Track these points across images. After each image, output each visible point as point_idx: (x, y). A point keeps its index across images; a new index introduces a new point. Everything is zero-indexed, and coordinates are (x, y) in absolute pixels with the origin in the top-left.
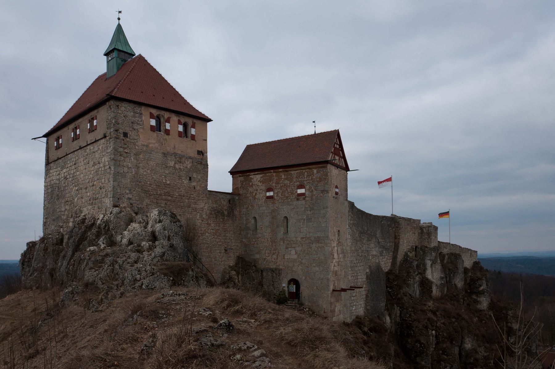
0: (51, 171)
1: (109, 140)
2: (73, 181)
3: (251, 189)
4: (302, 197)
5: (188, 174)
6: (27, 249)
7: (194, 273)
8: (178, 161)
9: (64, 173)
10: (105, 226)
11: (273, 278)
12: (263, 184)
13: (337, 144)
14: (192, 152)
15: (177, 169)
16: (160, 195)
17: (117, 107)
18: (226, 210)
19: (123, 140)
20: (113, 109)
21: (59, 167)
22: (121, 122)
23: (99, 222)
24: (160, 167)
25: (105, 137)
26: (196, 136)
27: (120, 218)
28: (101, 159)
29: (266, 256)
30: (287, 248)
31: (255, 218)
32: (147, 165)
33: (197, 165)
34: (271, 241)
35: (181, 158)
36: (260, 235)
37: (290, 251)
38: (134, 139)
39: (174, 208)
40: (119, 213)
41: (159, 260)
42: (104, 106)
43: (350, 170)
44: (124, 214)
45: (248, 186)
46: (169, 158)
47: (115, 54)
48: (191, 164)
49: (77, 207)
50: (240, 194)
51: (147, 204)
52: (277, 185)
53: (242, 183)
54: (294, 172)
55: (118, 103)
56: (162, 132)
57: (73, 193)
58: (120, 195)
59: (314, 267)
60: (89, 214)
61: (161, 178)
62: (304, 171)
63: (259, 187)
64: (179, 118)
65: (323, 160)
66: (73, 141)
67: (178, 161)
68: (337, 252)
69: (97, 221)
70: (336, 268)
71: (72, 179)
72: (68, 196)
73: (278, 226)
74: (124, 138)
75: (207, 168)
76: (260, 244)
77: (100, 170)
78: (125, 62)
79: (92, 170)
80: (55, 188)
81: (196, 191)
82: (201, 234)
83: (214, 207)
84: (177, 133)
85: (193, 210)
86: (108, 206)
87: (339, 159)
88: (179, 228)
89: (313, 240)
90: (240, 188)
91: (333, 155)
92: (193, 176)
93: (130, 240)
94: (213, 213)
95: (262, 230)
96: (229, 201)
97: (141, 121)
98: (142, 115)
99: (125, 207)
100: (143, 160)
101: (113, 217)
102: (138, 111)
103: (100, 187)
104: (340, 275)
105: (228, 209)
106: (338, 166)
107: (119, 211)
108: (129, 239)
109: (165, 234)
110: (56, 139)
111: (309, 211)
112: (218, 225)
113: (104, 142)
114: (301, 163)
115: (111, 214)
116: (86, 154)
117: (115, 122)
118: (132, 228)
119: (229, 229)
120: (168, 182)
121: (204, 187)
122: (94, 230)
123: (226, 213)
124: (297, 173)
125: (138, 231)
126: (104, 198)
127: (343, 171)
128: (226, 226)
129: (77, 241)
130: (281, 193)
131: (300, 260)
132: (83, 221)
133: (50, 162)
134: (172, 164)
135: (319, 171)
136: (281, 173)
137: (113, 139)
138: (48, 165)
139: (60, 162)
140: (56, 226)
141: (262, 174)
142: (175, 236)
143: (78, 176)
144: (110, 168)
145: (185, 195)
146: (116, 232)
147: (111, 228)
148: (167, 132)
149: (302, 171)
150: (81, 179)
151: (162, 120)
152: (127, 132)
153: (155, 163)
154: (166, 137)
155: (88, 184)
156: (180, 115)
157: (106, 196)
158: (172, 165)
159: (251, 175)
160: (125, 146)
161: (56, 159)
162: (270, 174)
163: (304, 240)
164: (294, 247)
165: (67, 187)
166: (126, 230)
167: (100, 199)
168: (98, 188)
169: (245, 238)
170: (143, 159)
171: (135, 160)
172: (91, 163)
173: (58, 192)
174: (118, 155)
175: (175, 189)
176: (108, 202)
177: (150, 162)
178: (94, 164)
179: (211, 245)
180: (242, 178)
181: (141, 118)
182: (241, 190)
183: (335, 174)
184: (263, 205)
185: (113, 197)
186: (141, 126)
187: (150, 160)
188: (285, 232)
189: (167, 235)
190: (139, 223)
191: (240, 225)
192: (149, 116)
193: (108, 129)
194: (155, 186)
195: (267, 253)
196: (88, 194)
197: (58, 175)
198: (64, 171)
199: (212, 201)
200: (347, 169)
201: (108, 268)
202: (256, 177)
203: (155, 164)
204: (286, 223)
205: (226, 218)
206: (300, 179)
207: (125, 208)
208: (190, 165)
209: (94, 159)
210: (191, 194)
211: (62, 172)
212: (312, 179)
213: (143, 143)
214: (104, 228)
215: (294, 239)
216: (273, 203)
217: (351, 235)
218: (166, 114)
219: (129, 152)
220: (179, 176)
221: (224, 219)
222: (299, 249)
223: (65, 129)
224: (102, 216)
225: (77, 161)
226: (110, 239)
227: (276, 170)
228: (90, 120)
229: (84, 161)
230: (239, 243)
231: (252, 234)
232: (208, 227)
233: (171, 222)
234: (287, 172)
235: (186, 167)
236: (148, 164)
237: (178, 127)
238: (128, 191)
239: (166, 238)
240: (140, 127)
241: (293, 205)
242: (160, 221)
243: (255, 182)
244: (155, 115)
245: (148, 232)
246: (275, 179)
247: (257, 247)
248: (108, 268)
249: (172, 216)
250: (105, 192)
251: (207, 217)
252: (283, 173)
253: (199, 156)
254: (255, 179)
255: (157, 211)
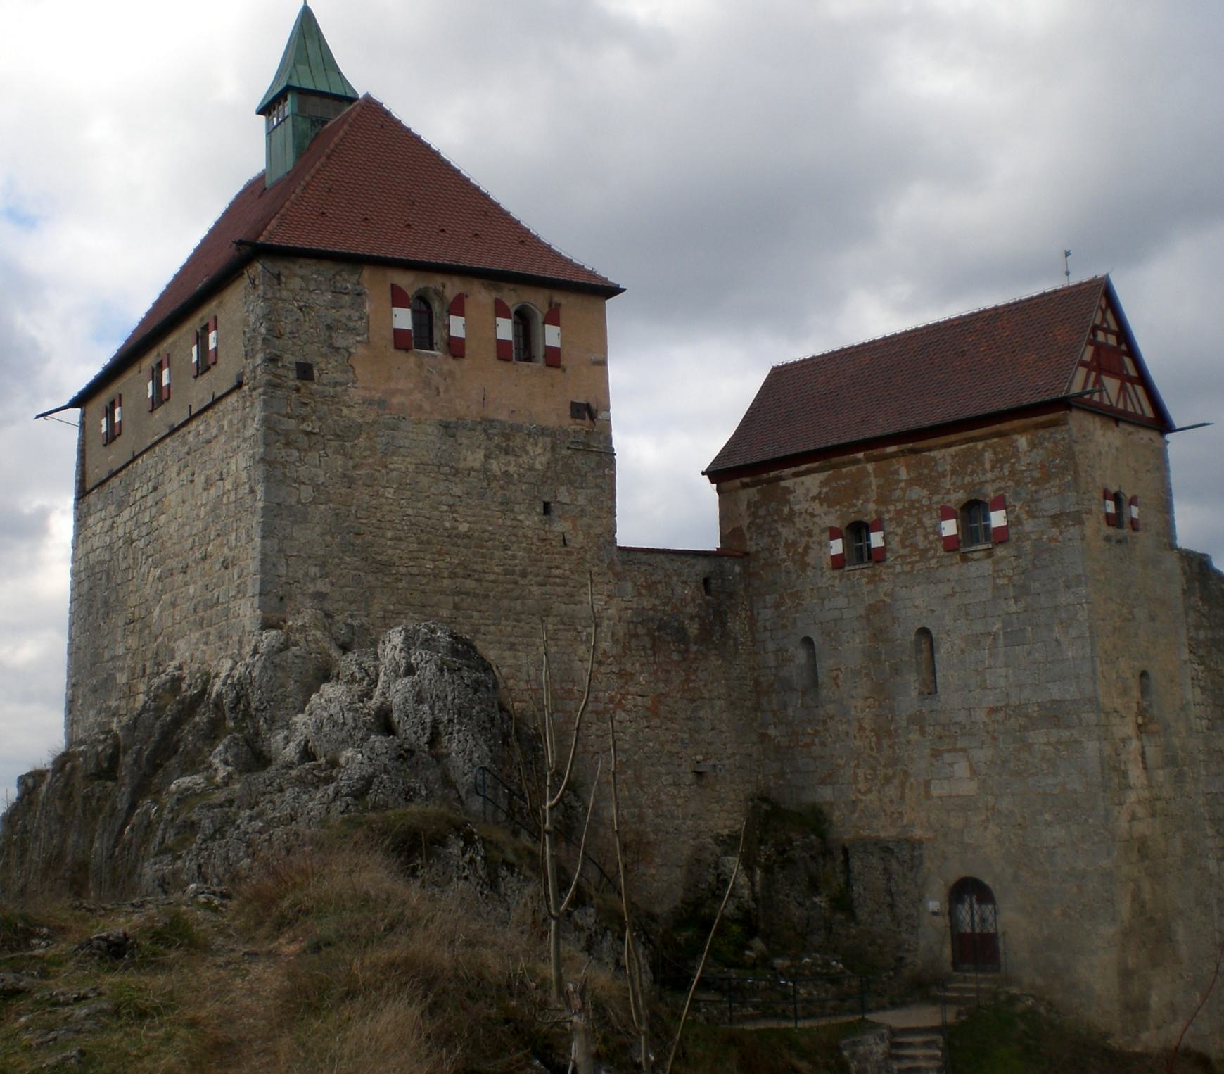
0: (91, 521)
1: (251, 396)
2: (150, 550)
3: (786, 533)
4: (980, 547)
5: (539, 492)
6: (20, 799)
7: (477, 854)
8: (498, 446)
9: (125, 523)
10: (238, 699)
11: (889, 880)
12: (831, 509)
13: (1107, 331)
14: (553, 413)
15: (495, 476)
16: (436, 575)
17: (275, 281)
18: (692, 618)
19: (298, 390)
20: (261, 288)
21: (113, 504)
22: (288, 330)
23: (217, 686)
24: (433, 475)
25: (239, 385)
26: (564, 353)
27: (283, 669)
28: (228, 464)
29: (859, 791)
30: (936, 754)
31: (808, 642)
32: (384, 471)
33: (570, 457)
34: (872, 730)
35: (507, 437)
36: (831, 708)
37: (951, 765)
38: (336, 384)
39: (488, 622)
40: (281, 650)
41: (348, 805)
42: (237, 283)
43: (1178, 425)
44: (298, 653)
45: (776, 521)
46: (465, 441)
47: (288, 107)
48: (548, 455)
49: (160, 639)
50: (747, 554)
51: (386, 611)
52: (883, 509)
53: (752, 509)
54: (943, 451)
55: (279, 266)
56: (438, 349)
57: (148, 591)
58: (287, 583)
59: (1049, 824)
60: (191, 661)
61: (436, 513)
62: (980, 445)
63: (815, 523)
64: (499, 296)
65: (1047, 398)
66: (151, 411)
67: (498, 446)
68: (1144, 761)
69: (213, 685)
70: (1141, 828)
71: (147, 543)
72: (135, 604)
73: (896, 670)
74: (298, 383)
75: (612, 463)
76: (835, 742)
77: (225, 500)
78: (323, 126)
79: (202, 505)
80: (99, 575)
81: (569, 553)
82: (597, 713)
83: (643, 608)
84: (492, 348)
85: (563, 623)
86: (248, 628)
87: (1123, 389)
88: (470, 691)
89: (1035, 715)
90: (749, 528)
91: (1093, 374)
92: (559, 499)
93: (306, 745)
94: (641, 631)
95: (838, 686)
96: (706, 582)
97: (361, 318)
98: (364, 297)
99: (304, 626)
100: (369, 456)
101: (259, 664)
102: (348, 285)
103: (223, 562)
104: (1165, 856)
105: (703, 614)
106: (1114, 416)
107: (282, 644)
108: (303, 743)
109: (421, 717)
110: (106, 408)
111: (1012, 602)
112: (661, 676)
113: (236, 404)
114: (965, 414)
115: (253, 655)
116: (186, 449)
117: (269, 331)
118: (323, 700)
119: (710, 691)
120: (464, 527)
121: (601, 535)
122: (200, 719)
123: (693, 629)
124: (953, 457)
125: (332, 712)
126: (234, 597)
127: (1145, 435)
128: (694, 681)
129: (147, 758)
130: (898, 538)
131: (990, 798)
132: (176, 681)
133: (88, 487)
134: (475, 459)
135: (1037, 441)
136: (894, 461)
137: (261, 390)
138: (81, 501)
139: (115, 485)
140: (99, 713)
141: (824, 471)
142: (455, 721)
143: (162, 530)
144: (252, 491)
145: (530, 569)
146: (271, 721)
147: (253, 705)
148: (456, 348)
149: (971, 444)
150: (170, 538)
151: (436, 307)
152: (309, 362)
153: (411, 463)
154: (452, 364)
155: (191, 553)
156: (503, 284)
157: (241, 591)
158: (477, 465)
159: (784, 480)
160: (304, 411)
161: (104, 478)
162: (854, 468)
163: (1000, 716)
164: (964, 750)
165: (130, 570)
166: (302, 711)
167: (223, 604)
168: (217, 568)
169: (775, 724)
170: (369, 453)
171: (339, 457)
172: (200, 480)
173: (107, 589)
174: (278, 444)
175: (489, 549)
176: (247, 612)
177: (395, 458)
178: (208, 484)
179: (636, 757)
180: (752, 493)
181: (362, 304)
182: (751, 539)
183: (1109, 445)
184: (837, 589)
185: (261, 594)
186: (359, 335)
187: (394, 453)
188: (926, 691)
189: (428, 720)
190: (348, 681)
191: (756, 674)
192: (389, 296)
193: (246, 359)
194: (415, 545)
195: (861, 777)
196: (192, 590)
197: (107, 533)
198: (126, 514)
199: (635, 584)
200: (1161, 423)
201: (204, 846)
202: (803, 483)
203: (413, 466)
204: (925, 654)
205: (694, 648)
206: (968, 479)
207: (303, 628)
208: (544, 459)
209: (208, 467)
210: (552, 564)
211: (118, 520)
212: (1013, 472)
213: (367, 394)
214: (233, 709)
215: (961, 717)
216: (875, 579)
217: (1203, 689)
218: (449, 284)
219: (317, 430)
220: (502, 504)
221: (687, 651)
222: (982, 755)
223: (131, 375)
224: (228, 664)
225: (161, 478)
226: (248, 745)
227: (876, 452)
228: (198, 334)
229: (179, 474)
230: (754, 743)
231: (802, 705)
232: (622, 687)
233: (441, 670)
234: (919, 455)
235: (531, 469)
236: (386, 467)
237: (496, 325)
238: (314, 570)
239: (423, 729)
240: (358, 338)
241: (948, 580)
242: (410, 670)
243: (800, 502)
244: (411, 293)
245: (366, 711)
246: (874, 487)
247: (823, 757)
248: (204, 846)
249: (457, 650)
250: (239, 577)
251: (617, 650)
252: (902, 459)
253: (578, 421)
254: (800, 491)
255: (401, 632)
